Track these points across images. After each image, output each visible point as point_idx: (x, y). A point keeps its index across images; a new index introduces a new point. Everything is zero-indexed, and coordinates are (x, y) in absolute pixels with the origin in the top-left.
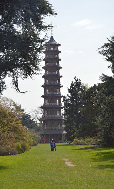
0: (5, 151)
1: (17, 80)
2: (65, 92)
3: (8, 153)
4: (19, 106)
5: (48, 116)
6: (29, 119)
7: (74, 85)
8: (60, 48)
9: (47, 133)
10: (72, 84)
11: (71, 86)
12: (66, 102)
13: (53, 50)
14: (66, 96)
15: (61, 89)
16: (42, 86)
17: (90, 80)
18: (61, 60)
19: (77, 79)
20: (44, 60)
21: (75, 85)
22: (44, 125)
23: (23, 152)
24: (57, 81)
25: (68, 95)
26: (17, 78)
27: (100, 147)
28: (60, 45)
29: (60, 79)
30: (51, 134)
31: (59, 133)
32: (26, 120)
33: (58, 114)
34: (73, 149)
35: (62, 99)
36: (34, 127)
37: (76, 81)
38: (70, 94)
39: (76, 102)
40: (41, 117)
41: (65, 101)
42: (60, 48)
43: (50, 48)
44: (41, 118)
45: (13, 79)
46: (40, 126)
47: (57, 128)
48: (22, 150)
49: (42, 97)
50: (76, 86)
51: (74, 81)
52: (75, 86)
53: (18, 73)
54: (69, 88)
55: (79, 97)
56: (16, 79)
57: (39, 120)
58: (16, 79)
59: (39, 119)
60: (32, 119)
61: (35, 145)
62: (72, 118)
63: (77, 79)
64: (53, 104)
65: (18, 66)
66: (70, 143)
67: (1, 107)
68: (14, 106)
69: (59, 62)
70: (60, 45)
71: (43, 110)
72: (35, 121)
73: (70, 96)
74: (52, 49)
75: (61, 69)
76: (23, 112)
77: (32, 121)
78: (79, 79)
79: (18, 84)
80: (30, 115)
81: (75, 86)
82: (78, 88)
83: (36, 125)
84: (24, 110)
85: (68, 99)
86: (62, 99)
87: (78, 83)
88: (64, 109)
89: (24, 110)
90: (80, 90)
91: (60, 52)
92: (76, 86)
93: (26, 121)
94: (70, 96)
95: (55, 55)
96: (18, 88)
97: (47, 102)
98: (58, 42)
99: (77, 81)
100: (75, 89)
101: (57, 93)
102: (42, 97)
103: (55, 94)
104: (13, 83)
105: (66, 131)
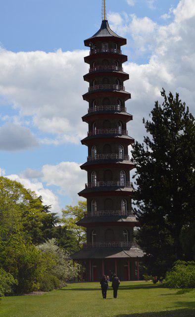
2: (137, 130)
8: (124, 50)
10: (156, 112)
14: (141, 141)
19: (171, 95)
28: (123, 41)
32: (43, 226)
34: (160, 294)
42: (124, 50)
51: (161, 100)
63: (171, 95)
64: (110, 183)
66: (155, 282)
67: (1, 203)
69: (127, 124)
70: (123, 41)
74: (105, 50)
78: (177, 95)
82: (176, 118)
84: (48, 208)
88: (135, 170)
93: (49, 229)
99: (170, 101)
100: (166, 122)
105: (142, 246)
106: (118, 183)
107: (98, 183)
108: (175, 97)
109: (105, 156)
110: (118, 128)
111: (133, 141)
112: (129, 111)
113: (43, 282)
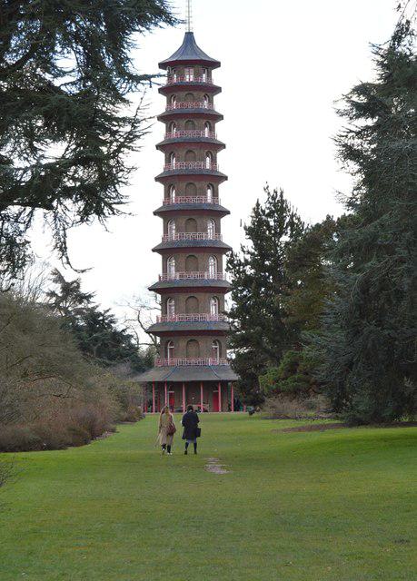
0: (32, 436)
1: (65, 236)
2: (234, 234)
3: (39, 442)
4: (72, 283)
5: (178, 278)
6: (111, 327)
7: (263, 212)
8: (217, 77)
9: (175, 379)
10: (257, 211)
11: (253, 215)
12: (238, 272)
13: (191, 79)
15: (224, 221)
16: (157, 179)
17: (325, 192)
18: (222, 146)
20: (161, 118)
21: (267, 211)
22: (161, 349)
23: (86, 443)
24: (209, 192)
25: (242, 248)
26: (64, 229)
27: (343, 425)
28: (216, 64)
29: (216, 124)
30: (185, 382)
31: (215, 379)
32: (98, 338)
33: (213, 310)
35: (225, 258)
36: (127, 356)
37: (270, 200)
38: (249, 244)
39: (271, 270)
40: (155, 322)
41: (234, 266)
42: (217, 77)
43: (182, 76)
44: (153, 326)
45: (54, 232)
46: (149, 353)
47: (210, 361)
48: (87, 432)
49: (155, 213)
50: (271, 220)
52: (269, 215)
53: (67, 212)
54: (249, 224)
55: (282, 255)
56: (61, 233)
57: (148, 332)
58: (61, 233)
59: (147, 326)
60: (119, 327)
61: (130, 420)
62: (258, 328)
64: (193, 275)
65: (68, 193)
68: (55, 281)
70: (216, 64)
71: (159, 296)
72: (130, 337)
73: (253, 251)
74: (189, 77)
75: (227, 216)
76: (89, 302)
77: (120, 338)
78: (282, 193)
79: (67, 245)
80: (112, 316)
81: (269, 215)
82: (280, 222)
83: (134, 349)
84: (90, 296)
85: (246, 260)
86: (225, 258)
87: (279, 206)
89: (90, 296)
90: (287, 227)
91: (219, 117)
92: (271, 220)
94: (253, 251)
95: (202, 101)
96: (67, 258)
97: (173, 269)
98: (213, 54)
99: (274, 198)
101: (209, 200)
102: (155, 213)
103: (202, 242)
104: (54, 244)
106: (206, 275)
107: (178, 274)
108: (279, 194)
109: (190, 235)
110: (205, 194)
111: (230, 249)
112: (224, 201)
113: (362, 316)
